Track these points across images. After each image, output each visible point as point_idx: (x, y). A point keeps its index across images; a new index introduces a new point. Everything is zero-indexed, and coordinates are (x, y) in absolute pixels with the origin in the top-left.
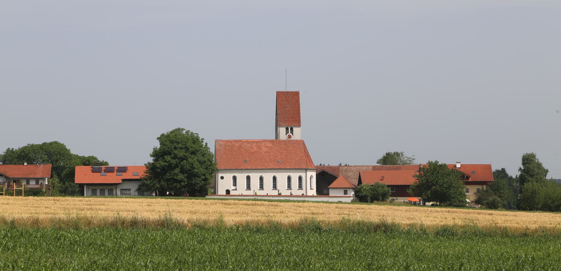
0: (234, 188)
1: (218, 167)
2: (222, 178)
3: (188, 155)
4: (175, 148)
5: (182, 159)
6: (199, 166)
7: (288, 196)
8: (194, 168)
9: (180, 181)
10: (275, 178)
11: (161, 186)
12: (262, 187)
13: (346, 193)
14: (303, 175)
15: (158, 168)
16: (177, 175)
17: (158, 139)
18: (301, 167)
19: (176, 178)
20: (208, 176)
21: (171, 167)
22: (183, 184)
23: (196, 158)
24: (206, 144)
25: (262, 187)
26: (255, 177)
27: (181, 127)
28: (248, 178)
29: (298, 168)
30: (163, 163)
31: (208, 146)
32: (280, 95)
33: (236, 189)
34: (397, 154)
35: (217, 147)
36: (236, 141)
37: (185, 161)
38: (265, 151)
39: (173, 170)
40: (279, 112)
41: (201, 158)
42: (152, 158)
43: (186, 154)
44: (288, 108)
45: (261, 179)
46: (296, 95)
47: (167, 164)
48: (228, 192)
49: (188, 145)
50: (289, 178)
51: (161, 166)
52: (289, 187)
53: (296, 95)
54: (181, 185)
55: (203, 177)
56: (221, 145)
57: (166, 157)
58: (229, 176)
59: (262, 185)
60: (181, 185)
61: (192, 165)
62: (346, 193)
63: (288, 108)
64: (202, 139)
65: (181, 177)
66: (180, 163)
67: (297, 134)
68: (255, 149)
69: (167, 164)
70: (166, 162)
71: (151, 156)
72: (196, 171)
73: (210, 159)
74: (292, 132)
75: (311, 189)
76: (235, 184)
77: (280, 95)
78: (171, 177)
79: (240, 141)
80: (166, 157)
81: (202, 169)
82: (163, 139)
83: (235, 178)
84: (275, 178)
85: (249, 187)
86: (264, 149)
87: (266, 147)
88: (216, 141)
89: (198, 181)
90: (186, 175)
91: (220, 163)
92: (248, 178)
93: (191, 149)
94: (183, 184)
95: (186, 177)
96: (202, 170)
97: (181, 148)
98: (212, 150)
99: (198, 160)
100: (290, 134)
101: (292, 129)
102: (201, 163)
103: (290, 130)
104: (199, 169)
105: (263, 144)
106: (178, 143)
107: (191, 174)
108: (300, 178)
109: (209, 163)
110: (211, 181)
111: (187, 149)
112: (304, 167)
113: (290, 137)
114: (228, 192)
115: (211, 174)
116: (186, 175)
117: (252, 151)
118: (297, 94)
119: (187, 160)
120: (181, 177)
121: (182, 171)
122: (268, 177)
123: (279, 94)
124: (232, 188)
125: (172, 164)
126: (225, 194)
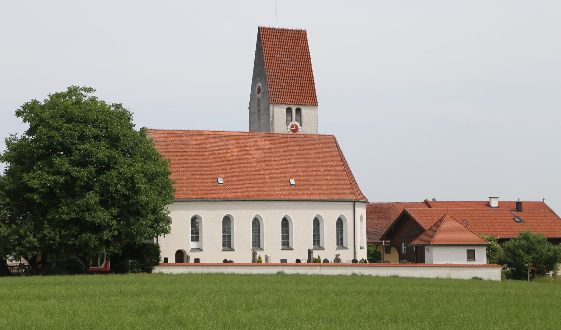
0: (194, 245)
4: (82, 138)
9: (97, 228)
10: (285, 223)
11: (42, 240)
13: (471, 256)
16: (88, 209)
17: (18, 114)
18: (343, 197)
21: (72, 188)
22: (106, 235)
28: (227, 220)
29: (336, 197)
32: (265, 36)
33: (200, 250)
38: (257, 158)
44: (283, 66)
45: (256, 223)
46: (298, 38)
47: (62, 179)
50: (317, 223)
53: (298, 38)
54: (100, 240)
57: (57, 161)
60: (100, 240)
62: (471, 256)
63: (283, 66)
67: (320, 120)
68: (235, 151)
69: (61, 179)
70: (59, 173)
71: (5, 158)
74: (299, 119)
76: (196, 236)
77: (265, 36)
78: (73, 215)
79: (199, 133)
80: (57, 161)
84: (285, 223)
86: (256, 154)
87: (258, 148)
90: (115, 211)
91: (178, 178)
95: (115, 218)
97: (96, 138)
100: (294, 122)
101: (298, 111)
108: (340, 223)
112: (350, 197)
113: (295, 130)
116: (115, 211)
117: (228, 156)
120: (101, 216)
123: (263, 33)
124: (188, 246)
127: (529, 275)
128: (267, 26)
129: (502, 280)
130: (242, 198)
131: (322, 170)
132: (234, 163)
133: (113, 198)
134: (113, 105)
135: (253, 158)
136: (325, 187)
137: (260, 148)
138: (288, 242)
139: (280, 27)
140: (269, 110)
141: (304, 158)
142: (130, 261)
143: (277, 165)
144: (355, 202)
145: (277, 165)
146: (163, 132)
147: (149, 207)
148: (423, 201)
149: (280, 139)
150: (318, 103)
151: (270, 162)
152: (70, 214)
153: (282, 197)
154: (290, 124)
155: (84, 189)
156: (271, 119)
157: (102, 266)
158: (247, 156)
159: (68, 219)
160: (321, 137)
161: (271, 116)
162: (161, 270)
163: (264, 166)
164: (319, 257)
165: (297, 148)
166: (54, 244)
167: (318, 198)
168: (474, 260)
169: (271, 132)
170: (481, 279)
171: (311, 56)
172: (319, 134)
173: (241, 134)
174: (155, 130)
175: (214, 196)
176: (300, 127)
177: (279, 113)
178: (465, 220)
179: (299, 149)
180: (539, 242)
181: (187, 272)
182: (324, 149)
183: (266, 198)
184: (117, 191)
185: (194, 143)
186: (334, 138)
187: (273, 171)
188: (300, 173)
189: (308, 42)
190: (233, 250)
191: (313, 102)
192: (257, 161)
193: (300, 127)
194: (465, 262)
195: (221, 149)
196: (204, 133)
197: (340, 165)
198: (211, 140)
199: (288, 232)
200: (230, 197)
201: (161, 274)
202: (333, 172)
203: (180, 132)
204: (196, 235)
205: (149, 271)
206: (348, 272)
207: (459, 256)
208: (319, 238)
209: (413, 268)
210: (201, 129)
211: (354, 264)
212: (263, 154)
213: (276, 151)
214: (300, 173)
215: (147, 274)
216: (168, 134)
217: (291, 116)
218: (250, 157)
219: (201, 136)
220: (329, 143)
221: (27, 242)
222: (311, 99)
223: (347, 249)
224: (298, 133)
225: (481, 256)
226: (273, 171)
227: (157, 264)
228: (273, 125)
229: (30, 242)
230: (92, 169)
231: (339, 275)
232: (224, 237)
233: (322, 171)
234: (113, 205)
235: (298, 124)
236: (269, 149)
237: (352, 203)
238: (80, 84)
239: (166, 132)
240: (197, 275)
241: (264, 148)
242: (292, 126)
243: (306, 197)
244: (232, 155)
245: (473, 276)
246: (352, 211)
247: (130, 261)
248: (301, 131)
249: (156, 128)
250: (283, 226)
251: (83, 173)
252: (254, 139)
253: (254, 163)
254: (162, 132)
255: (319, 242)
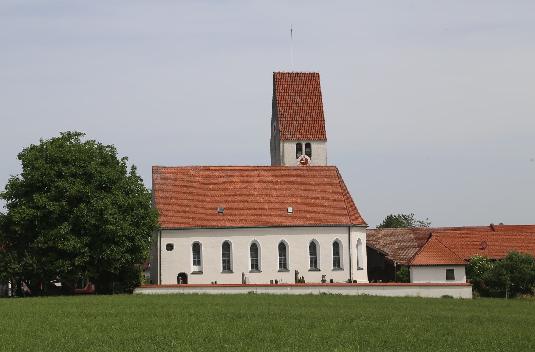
0: (195, 268)
1: (161, 220)
2: (170, 247)
3: (89, 190)
4: (60, 175)
5: (75, 200)
6: (119, 216)
7: (291, 286)
8: (107, 222)
9: (71, 255)
10: (283, 247)
11: (24, 267)
12: (255, 266)
13: (450, 275)
14: (342, 238)
15: (18, 224)
18: (338, 222)
19: (60, 246)
20: (139, 242)
21: (48, 221)
22: (78, 261)
23: (109, 200)
24: (134, 168)
25: (255, 266)
26: (241, 244)
27: (73, 130)
28: (227, 246)
29: (331, 223)
30: (28, 211)
31: (138, 173)
33: (200, 272)
34: (405, 218)
35: (158, 181)
36: (197, 169)
37: (82, 205)
38: (258, 188)
39: (53, 226)
40: (280, 112)
41: (121, 198)
42: (5, 202)
43: (87, 189)
44: (297, 104)
45: (254, 248)
47: (39, 213)
48: (183, 277)
49: (92, 167)
50: (313, 247)
51: (23, 219)
52: (314, 265)
53: (313, 79)
54: (73, 265)
55: (128, 244)
56: (167, 179)
58: (183, 244)
59: (257, 261)
60: (73, 265)
61: (102, 215)
62: (450, 275)
63: (297, 104)
64: (124, 159)
65: (73, 243)
66: (71, 212)
67: (321, 155)
68: (238, 184)
69: (39, 213)
70: (37, 208)
71: (5, 196)
72: (110, 228)
73: (143, 201)
74: (309, 152)
75: (359, 269)
76: (197, 260)
78: (50, 244)
79: (206, 168)
80: (36, 196)
81: (125, 225)
82: (32, 158)
83: (197, 248)
84: (283, 247)
85: (227, 267)
86: (258, 185)
87: (261, 180)
88: (155, 169)
89: (117, 254)
90: (86, 240)
91: (165, 209)
92: (227, 246)
93: (97, 178)
94: (78, 261)
95: (86, 245)
96: (126, 227)
97: (74, 176)
98: (147, 184)
99: (115, 204)
101: (308, 146)
102: (124, 210)
103: (304, 149)
104: (118, 225)
105: (255, 175)
106: (66, 163)
107: (99, 238)
108: (336, 246)
109: (143, 211)
110: (147, 253)
111: (88, 177)
112: (345, 222)
114: (183, 277)
115: (145, 236)
116: (86, 240)
117: (231, 188)
118: (314, 78)
119: (89, 203)
120: (73, 243)
121: (78, 230)
122: (269, 244)
125: (51, 212)
126: (176, 283)
127: (507, 294)
128: (281, 71)
129: (473, 298)
130: (239, 225)
131: (320, 198)
132: (236, 194)
133: (85, 228)
134: (109, 146)
135: (255, 189)
136: (321, 214)
137: (263, 180)
138: (257, 265)
139: (294, 71)
140: (279, 146)
141: (304, 188)
142: (114, 283)
143: (277, 195)
144: (349, 227)
145: (277, 195)
146: (173, 168)
147: (118, 237)
148: (489, 225)
149: (283, 172)
150: (327, 138)
151: (270, 192)
152: (47, 243)
153: (278, 224)
154: (300, 158)
155: (79, 220)
156: (281, 154)
157: (86, 289)
158: (249, 187)
159: (45, 247)
160: (323, 168)
161: (281, 151)
162: (140, 292)
163: (264, 196)
164: (303, 278)
165: (298, 179)
166: (33, 270)
167: (313, 223)
168: (454, 279)
169: (282, 165)
170: (451, 297)
171: (322, 96)
172: (328, 165)
173: (245, 168)
174: (166, 167)
175: (213, 224)
176: (309, 160)
177: (289, 149)
178: (485, 242)
179: (301, 180)
180: (522, 261)
181: (147, 293)
182: (325, 179)
183: (262, 224)
184: (87, 222)
185: (201, 177)
186: (336, 169)
187: (273, 200)
188: (299, 201)
189: (321, 83)
190: (232, 272)
191: (322, 137)
192: (258, 191)
193: (309, 160)
194: (444, 282)
195: (225, 182)
196: (211, 168)
197: (340, 193)
198: (217, 174)
199: (285, 255)
200: (229, 225)
201: (141, 295)
202: (331, 200)
203: (189, 168)
204: (183, 260)
205: (130, 292)
206: (316, 291)
207: (439, 276)
208: (316, 260)
209: (382, 287)
210: (208, 165)
211: (350, 284)
212: (265, 185)
213: (277, 182)
214: (299, 201)
215: (127, 295)
216: (177, 170)
217: (301, 150)
218: (252, 189)
219: (207, 171)
220: (332, 175)
221: (11, 268)
222: (321, 135)
223: (343, 270)
224: (308, 165)
225: (461, 276)
226: (273, 200)
227: (138, 285)
228: (283, 159)
229: (13, 269)
230: (64, 203)
231: (406, 297)
232: (224, 261)
233: (324, 201)
234: (85, 235)
235: (308, 157)
236: (271, 181)
237: (347, 228)
238: (66, 129)
239: (175, 169)
240: (274, 296)
241: (266, 180)
242: (302, 160)
243: (301, 223)
244: (235, 187)
245: (443, 294)
246: (347, 235)
247: (114, 283)
248: (311, 163)
249: (167, 166)
250: (280, 250)
251: (55, 207)
252: (258, 172)
253: (255, 194)
254: (172, 169)
255: (316, 264)
